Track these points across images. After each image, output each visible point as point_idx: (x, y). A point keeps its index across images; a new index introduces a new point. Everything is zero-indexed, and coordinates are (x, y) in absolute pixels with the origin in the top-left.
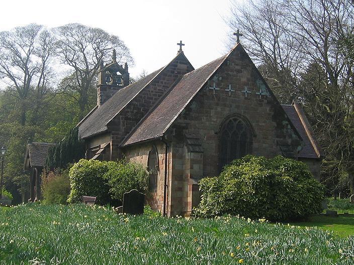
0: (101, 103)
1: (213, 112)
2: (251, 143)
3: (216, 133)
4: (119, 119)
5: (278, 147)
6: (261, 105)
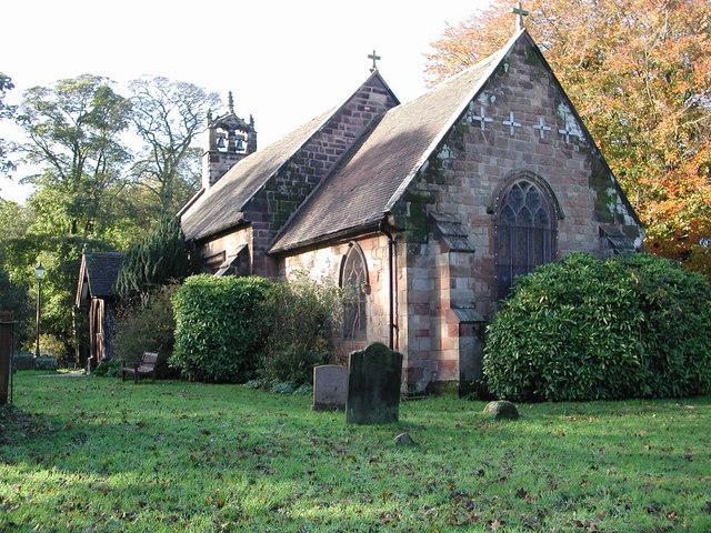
0: (212, 183)
1: (481, 167)
2: (555, 233)
3: (490, 212)
4: (264, 197)
5: (605, 241)
6: (569, 156)
